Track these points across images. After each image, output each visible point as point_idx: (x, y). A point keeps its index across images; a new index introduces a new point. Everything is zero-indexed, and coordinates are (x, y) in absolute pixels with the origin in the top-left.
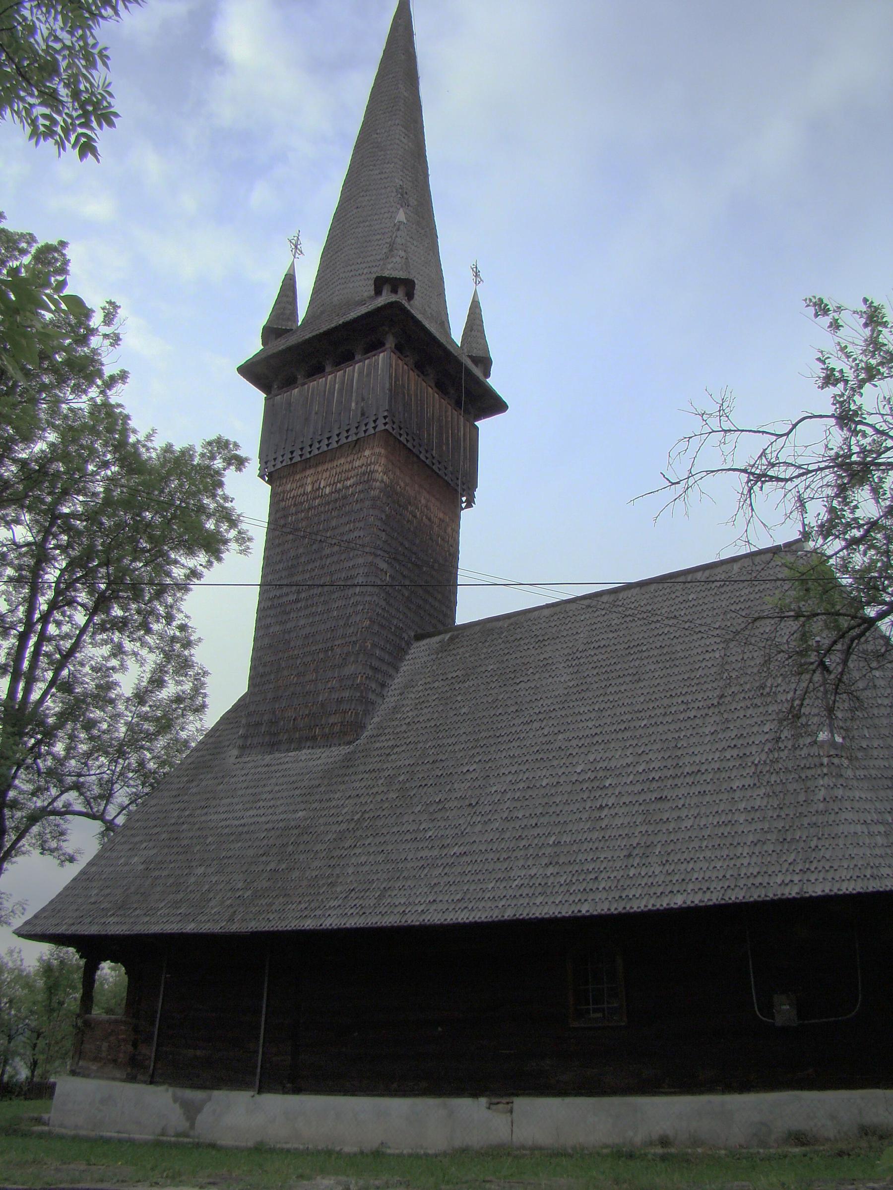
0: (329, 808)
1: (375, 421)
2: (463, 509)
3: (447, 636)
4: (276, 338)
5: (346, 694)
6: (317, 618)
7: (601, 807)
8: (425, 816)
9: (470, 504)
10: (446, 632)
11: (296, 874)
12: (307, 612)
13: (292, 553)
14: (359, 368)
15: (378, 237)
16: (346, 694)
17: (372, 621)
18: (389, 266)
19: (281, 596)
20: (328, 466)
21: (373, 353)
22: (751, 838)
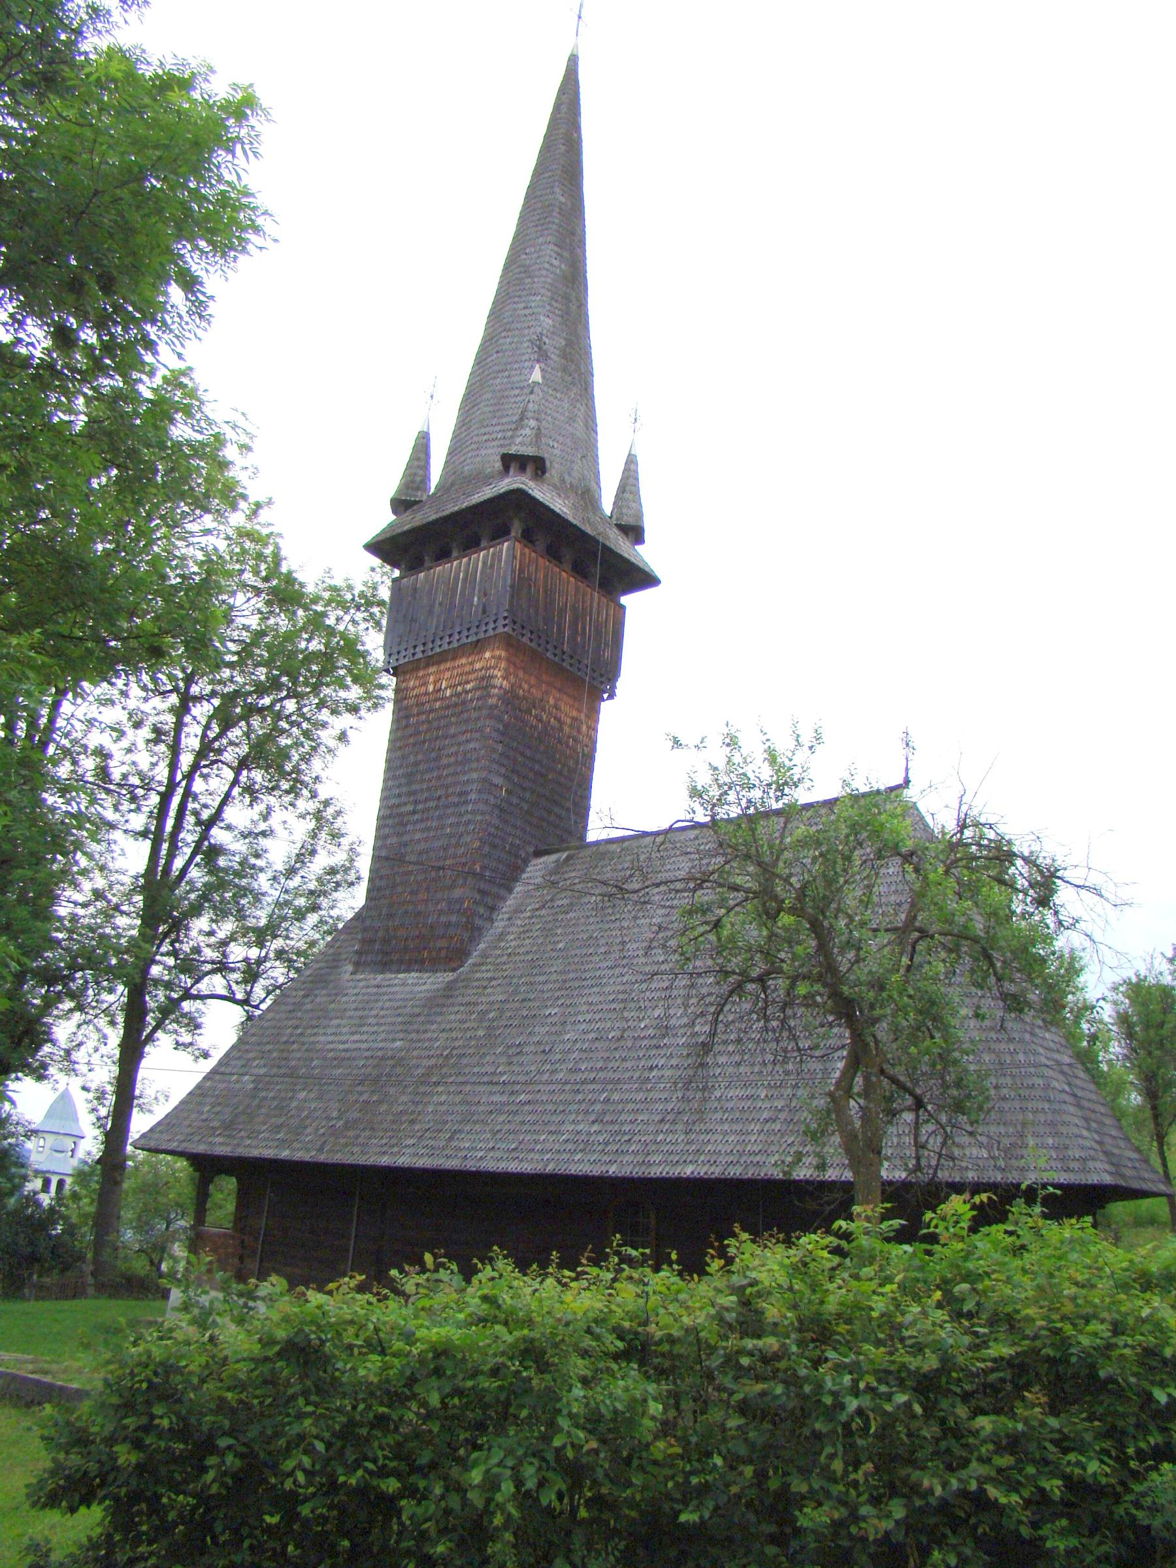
0: (423, 1040)
3: (565, 855)
4: (406, 510)
5: (454, 918)
7: (651, 1068)
8: (504, 1059)
10: (564, 850)
11: (384, 1107)
12: (423, 825)
13: (412, 759)
15: (517, 392)
16: (454, 918)
18: (518, 440)
22: (765, 1115)
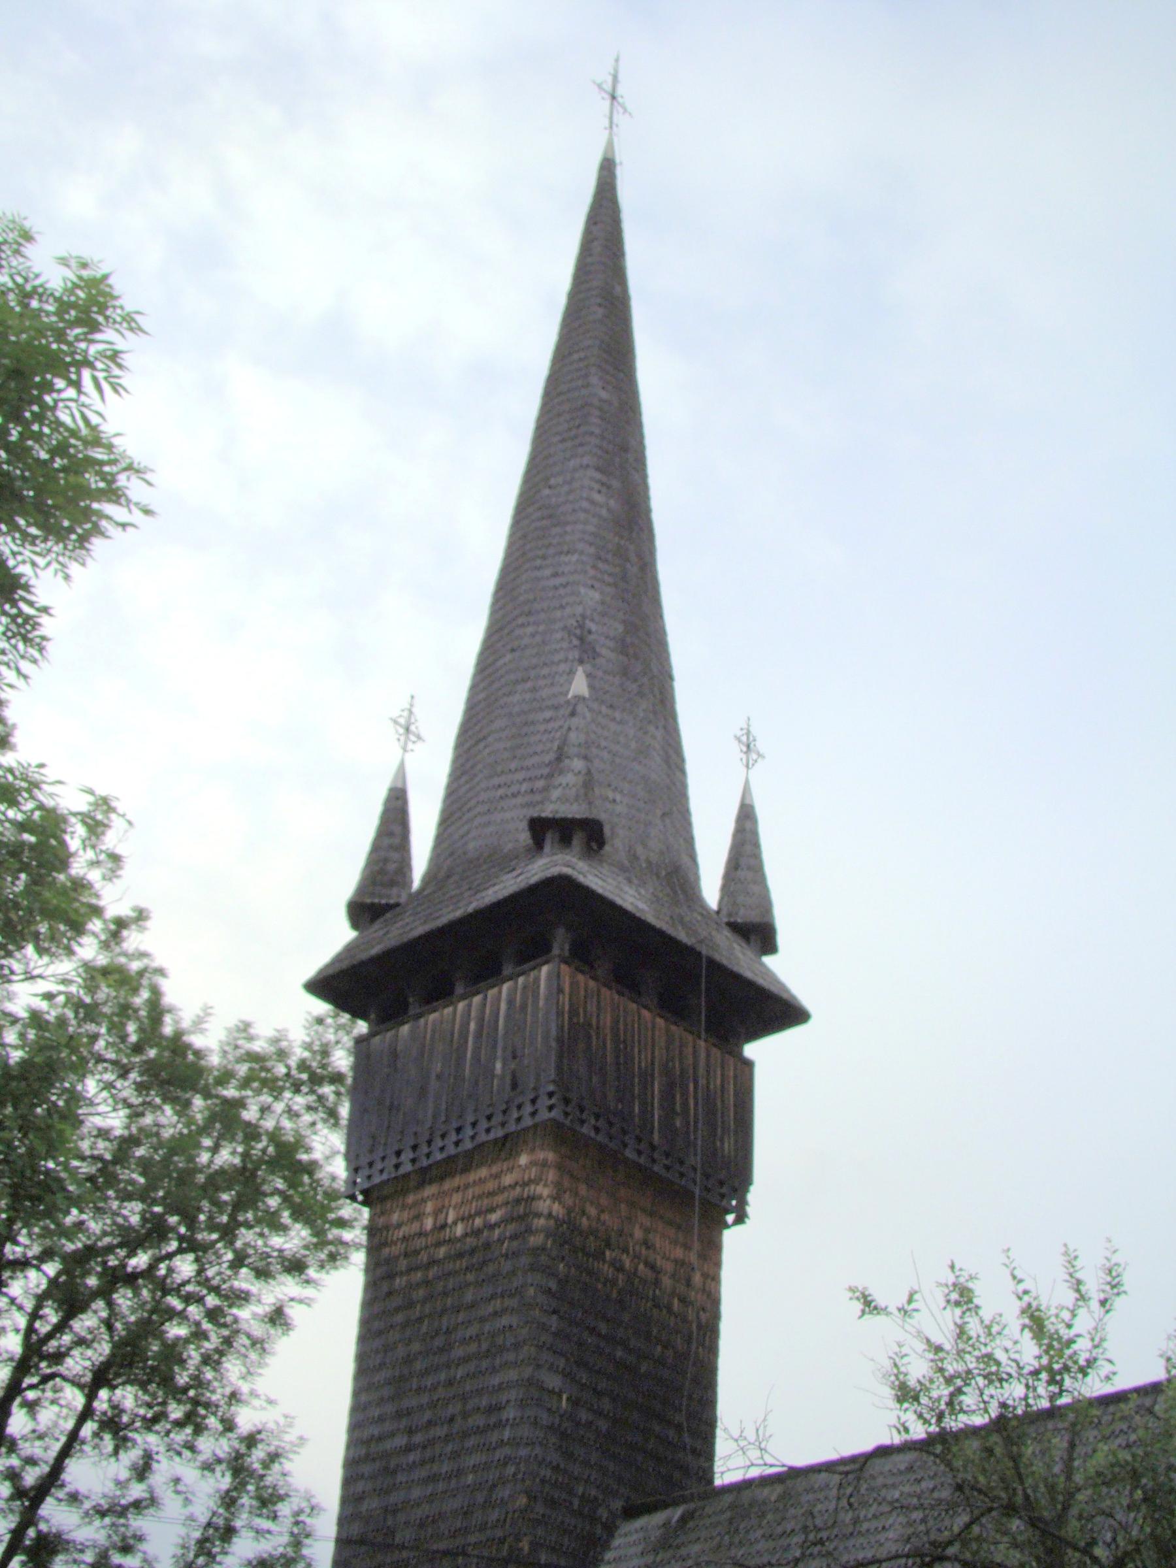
1: (533, 1101)
2: (727, 1226)
3: (678, 1512)
6: (441, 1486)
9: (741, 1219)
10: (675, 1503)
12: (424, 1473)
13: (401, 1351)
14: (509, 989)
15: (548, 714)
17: (532, 1498)
19: (380, 1439)
20: (457, 1181)
21: (532, 963)
